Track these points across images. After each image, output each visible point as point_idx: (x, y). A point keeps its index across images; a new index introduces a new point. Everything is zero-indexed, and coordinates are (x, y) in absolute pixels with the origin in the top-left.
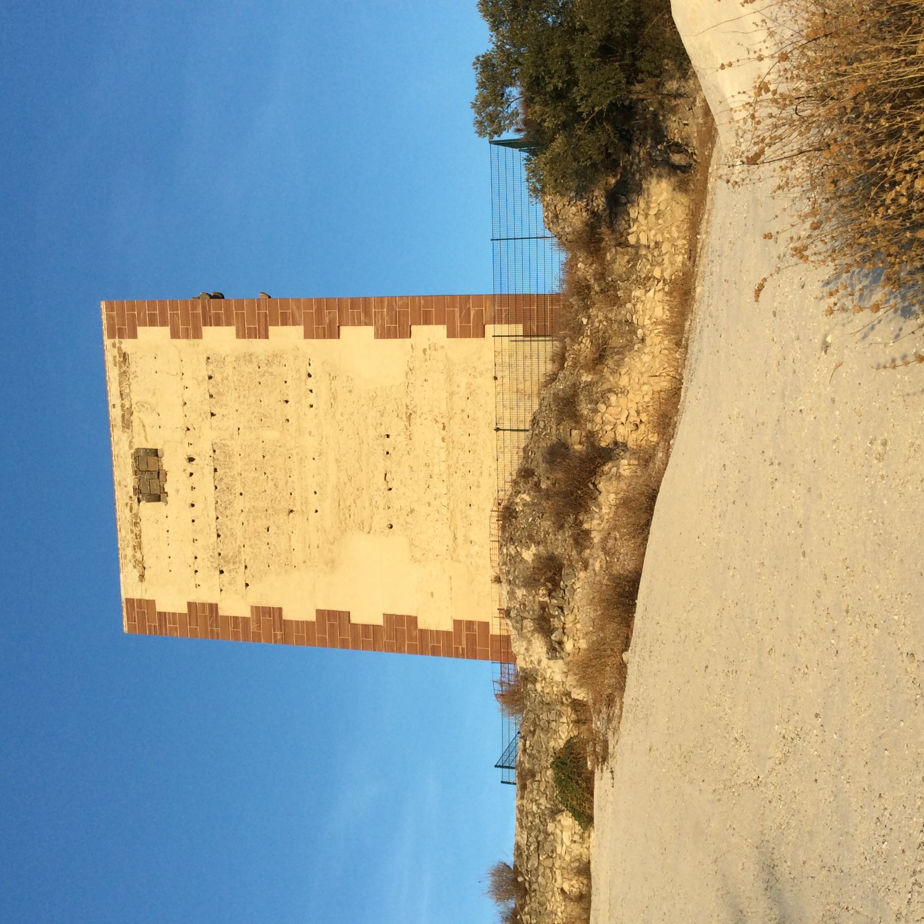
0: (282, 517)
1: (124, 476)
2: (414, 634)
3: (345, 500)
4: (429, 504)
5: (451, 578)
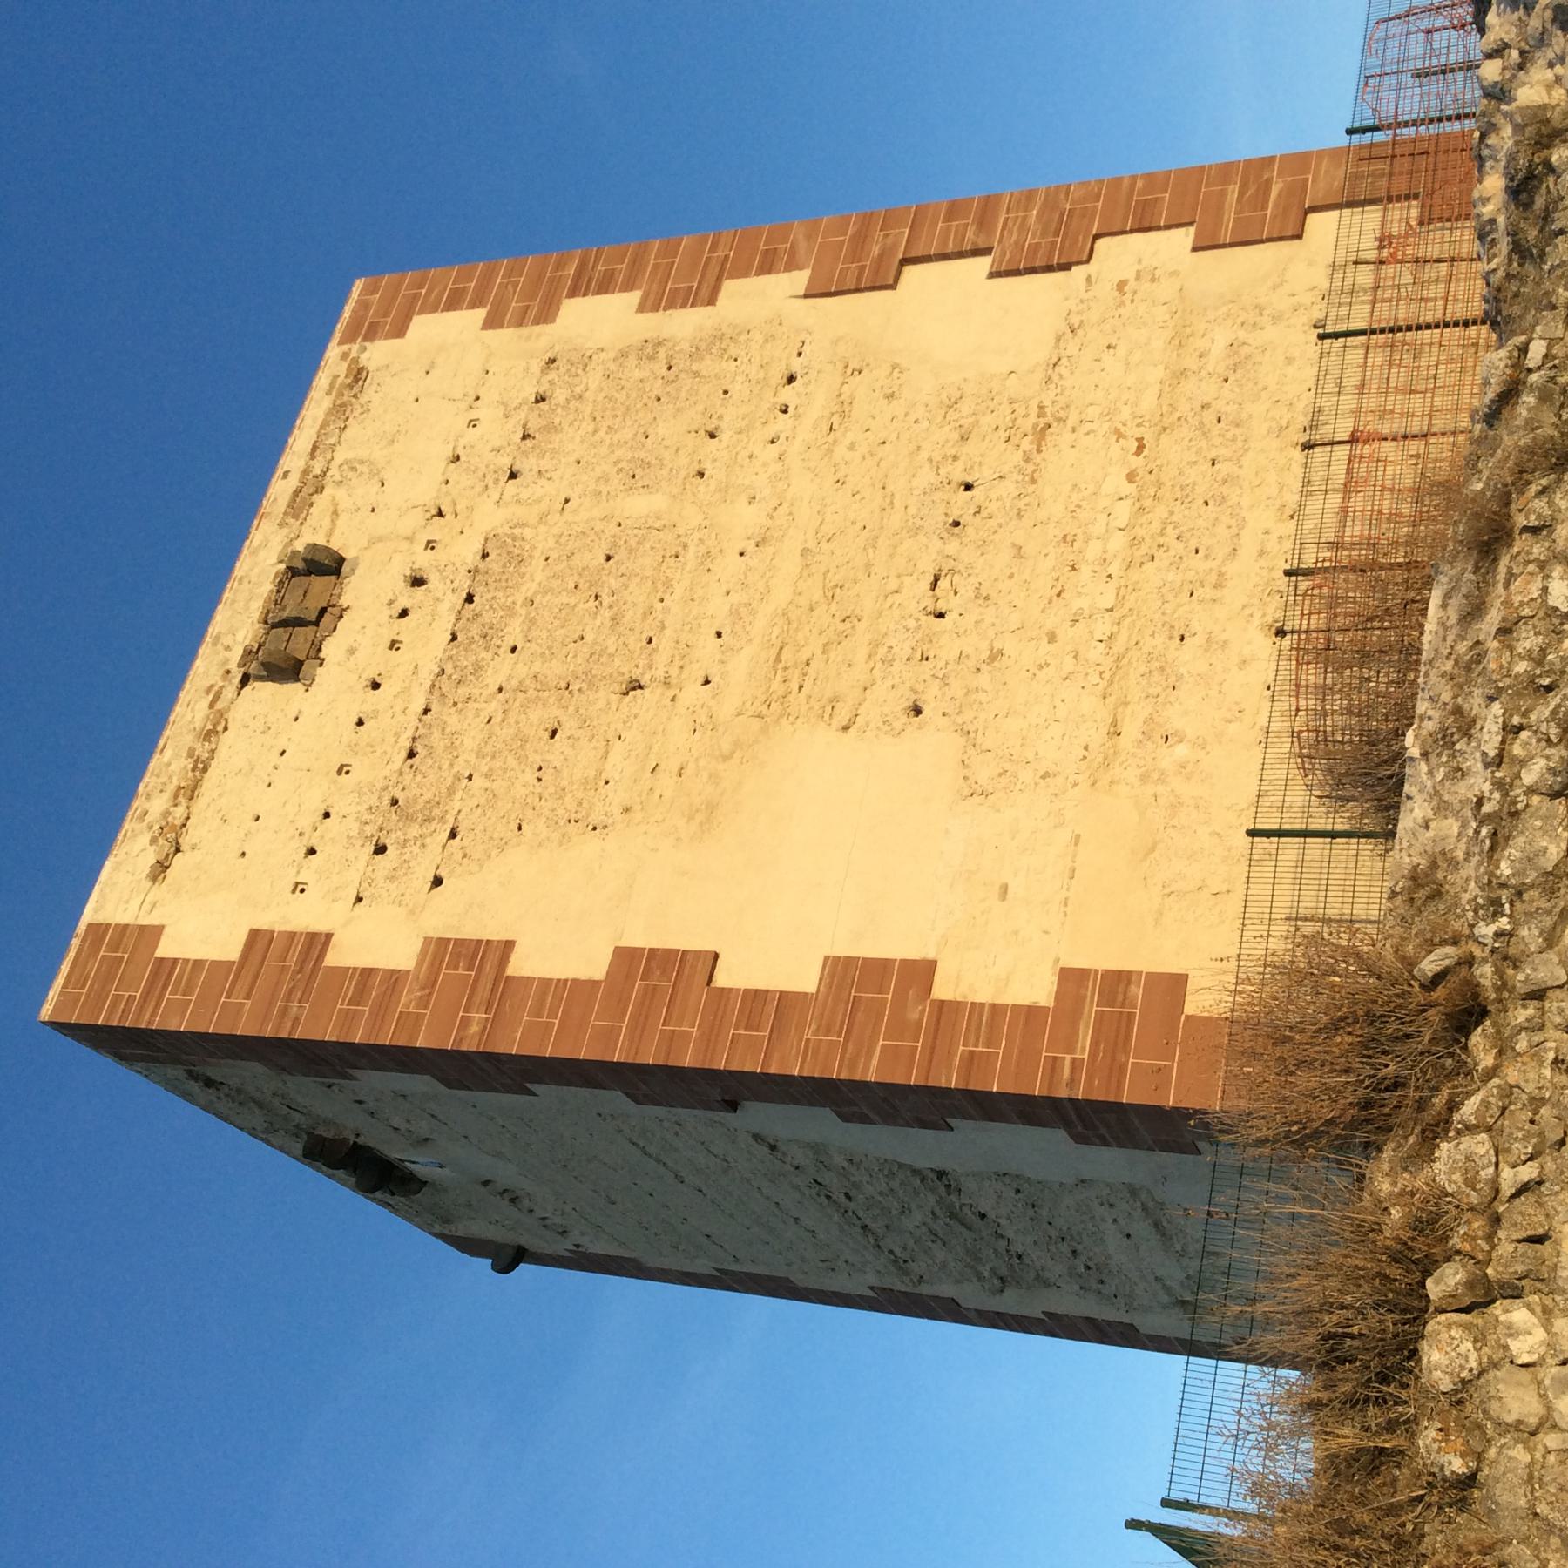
0: (605, 695)
1: (237, 621)
3: (799, 648)
4: (1052, 638)
5: (1077, 840)
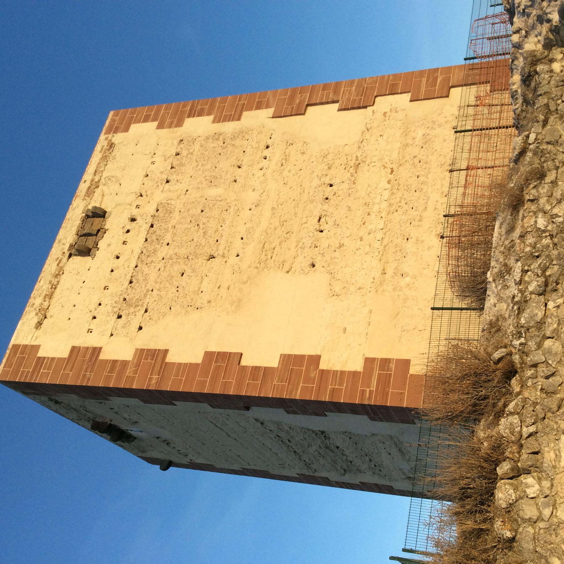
1: (67, 234)
2: (312, 375)
3: (271, 243)
4: (361, 239)
